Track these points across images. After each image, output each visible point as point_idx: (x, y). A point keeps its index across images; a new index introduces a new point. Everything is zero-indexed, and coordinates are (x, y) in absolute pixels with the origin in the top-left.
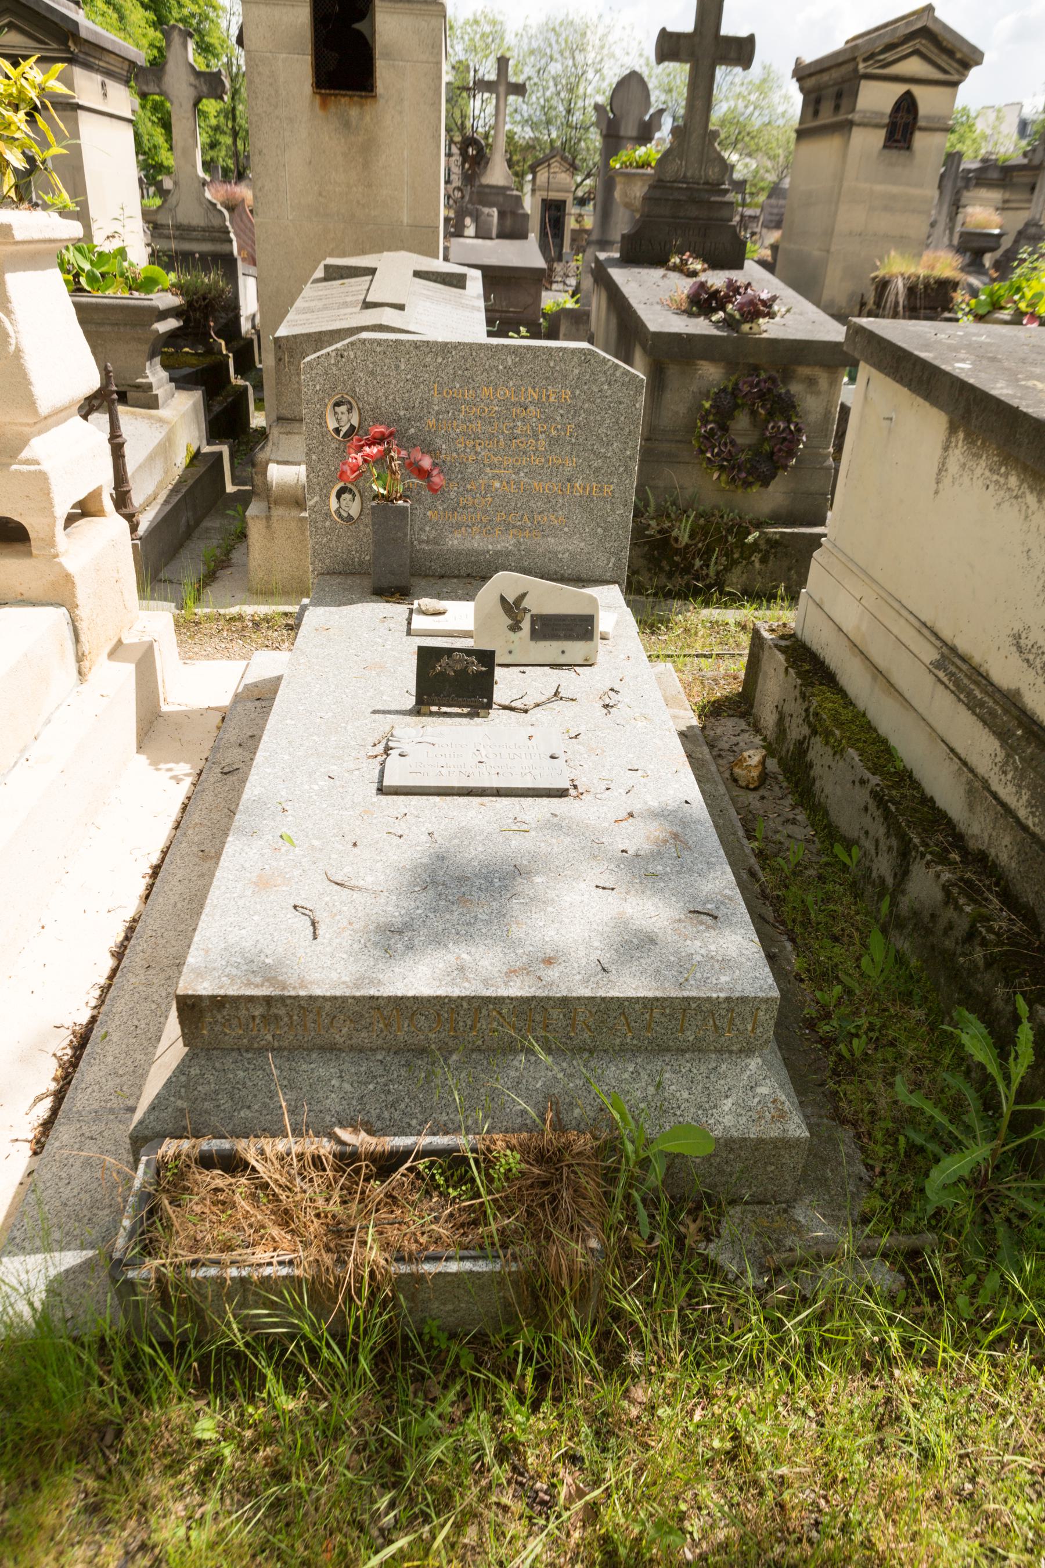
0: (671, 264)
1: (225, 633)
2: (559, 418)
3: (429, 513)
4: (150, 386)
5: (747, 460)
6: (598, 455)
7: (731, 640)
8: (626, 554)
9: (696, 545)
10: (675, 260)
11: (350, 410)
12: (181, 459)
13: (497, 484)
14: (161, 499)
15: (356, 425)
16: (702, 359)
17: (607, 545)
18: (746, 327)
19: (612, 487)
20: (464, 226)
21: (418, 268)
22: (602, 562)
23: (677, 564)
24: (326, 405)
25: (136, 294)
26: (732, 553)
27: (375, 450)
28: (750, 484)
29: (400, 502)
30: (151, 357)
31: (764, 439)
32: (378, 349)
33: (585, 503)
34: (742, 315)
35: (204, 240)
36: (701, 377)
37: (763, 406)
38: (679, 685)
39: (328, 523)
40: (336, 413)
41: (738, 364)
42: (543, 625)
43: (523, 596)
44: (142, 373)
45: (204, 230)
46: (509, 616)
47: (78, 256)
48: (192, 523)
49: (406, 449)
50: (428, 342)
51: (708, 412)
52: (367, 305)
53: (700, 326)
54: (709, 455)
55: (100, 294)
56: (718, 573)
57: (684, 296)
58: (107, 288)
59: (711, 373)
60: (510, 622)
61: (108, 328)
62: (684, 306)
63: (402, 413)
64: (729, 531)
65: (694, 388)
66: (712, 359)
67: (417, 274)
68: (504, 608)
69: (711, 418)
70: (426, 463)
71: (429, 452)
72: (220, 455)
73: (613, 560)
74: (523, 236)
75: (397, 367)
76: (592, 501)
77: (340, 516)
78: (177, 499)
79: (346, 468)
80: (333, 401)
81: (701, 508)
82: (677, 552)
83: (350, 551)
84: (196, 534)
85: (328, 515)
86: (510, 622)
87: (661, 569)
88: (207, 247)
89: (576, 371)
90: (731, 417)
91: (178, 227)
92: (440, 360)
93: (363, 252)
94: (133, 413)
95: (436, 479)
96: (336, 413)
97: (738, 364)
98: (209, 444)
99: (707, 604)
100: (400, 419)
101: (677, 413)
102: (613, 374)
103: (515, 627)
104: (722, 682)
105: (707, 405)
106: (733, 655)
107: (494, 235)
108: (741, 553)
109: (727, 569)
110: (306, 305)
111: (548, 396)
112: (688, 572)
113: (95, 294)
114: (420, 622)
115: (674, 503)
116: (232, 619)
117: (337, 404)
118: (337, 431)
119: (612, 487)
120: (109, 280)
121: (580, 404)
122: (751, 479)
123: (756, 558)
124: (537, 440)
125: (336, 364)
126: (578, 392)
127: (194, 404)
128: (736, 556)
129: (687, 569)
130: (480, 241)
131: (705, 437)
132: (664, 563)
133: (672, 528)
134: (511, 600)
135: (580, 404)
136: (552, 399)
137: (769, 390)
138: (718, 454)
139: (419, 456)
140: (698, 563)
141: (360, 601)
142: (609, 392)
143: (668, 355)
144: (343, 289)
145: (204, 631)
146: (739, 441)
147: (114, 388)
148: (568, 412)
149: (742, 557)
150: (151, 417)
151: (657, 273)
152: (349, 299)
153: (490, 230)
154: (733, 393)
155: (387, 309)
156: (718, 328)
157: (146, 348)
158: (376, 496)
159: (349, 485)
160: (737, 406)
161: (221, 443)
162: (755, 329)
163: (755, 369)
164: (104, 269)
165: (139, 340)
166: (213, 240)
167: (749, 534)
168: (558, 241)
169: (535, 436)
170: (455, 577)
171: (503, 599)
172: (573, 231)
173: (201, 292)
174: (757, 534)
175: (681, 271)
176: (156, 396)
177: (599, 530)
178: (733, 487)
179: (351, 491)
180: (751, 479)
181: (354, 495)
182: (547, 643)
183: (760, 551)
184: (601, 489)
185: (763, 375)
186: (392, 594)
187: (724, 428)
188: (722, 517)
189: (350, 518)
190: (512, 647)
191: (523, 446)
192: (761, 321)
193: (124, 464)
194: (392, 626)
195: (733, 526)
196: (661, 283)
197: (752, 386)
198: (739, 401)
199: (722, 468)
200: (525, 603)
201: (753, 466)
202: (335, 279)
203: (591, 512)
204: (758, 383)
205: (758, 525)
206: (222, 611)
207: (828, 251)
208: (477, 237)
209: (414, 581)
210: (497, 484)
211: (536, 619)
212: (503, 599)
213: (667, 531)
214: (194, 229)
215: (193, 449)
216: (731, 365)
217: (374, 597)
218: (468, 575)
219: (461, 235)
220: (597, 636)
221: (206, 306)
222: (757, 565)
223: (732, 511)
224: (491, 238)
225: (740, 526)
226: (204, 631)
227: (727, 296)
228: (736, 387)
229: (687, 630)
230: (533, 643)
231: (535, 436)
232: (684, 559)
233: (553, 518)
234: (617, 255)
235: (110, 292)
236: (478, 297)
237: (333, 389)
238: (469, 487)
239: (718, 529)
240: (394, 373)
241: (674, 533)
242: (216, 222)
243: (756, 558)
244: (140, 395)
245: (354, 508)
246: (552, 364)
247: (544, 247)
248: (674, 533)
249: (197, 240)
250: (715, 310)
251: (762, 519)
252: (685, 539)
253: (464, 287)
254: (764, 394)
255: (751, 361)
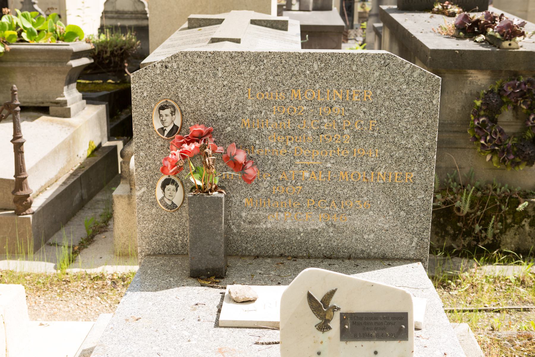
0: (435, 9)
1: (88, 290)
2: (362, 115)
3: (245, 201)
4: (65, 103)
5: (514, 145)
6: (399, 146)
7: (513, 294)
8: (428, 234)
9: (475, 213)
10: (438, 6)
11: (173, 113)
12: (83, 152)
13: (306, 174)
14: (60, 182)
15: (179, 125)
16: (475, 68)
17: (410, 227)
18: (506, 44)
19: (413, 175)
20: (292, 4)
21: (254, 18)
22: (405, 243)
23: (460, 229)
24: (152, 109)
25: (60, 42)
26: (506, 219)
27: (193, 146)
28: (518, 164)
29: (215, 194)
30: (69, 82)
31: (526, 128)
32: (198, 60)
33: (388, 189)
34: (502, 35)
35: (131, 19)
36: (471, 82)
37: (524, 103)
38: (479, 347)
39: (154, 211)
40: (161, 116)
41: (501, 71)
42: (353, 323)
43: (332, 293)
44: (61, 94)
45: (132, 13)
46: (318, 315)
47: (23, 19)
48: (85, 197)
49: (223, 145)
50: (242, 53)
51: (479, 109)
52: (214, 40)
53: (467, 45)
54: (483, 142)
55: (35, 43)
56: (494, 235)
57: (451, 26)
58: (40, 39)
59: (479, 79)
60: (318, 321)
61: (38, 65)
62: (453, 32)
63: (219, 114)
64: (503, 201)
65: (466, 91)
66: (480, 68)
67: (253, 22)
68: (312, 307)
69: (482, 113)
70: (241, 157)
71: (244, 147)
72: (115, 147)
73: (415, 240)
74: (329, 8)
75: (215, 75)
76: (395, 187)
77: (166, 206)
78: (73, 180)
79: (167, 163)
80: (158, 105)
81: (478, 184)
82: (459, 219)
83: (173, 235)
84: (88, 205)
85: (154, 203)
86: (318, 321)
87: (447, 233)
88: (133, 23)
89: (377, 74)
90: (499, 112)
91: (117, 12)
92: (253, 68)
93: (220, 13)
94: (51, 121)
95: (250, 171)
96: (161, 116)
97: (501, 71)
98: (109, 140)
99: (491, 261)
100: (218, 119)
101: (453, 110)
102: (411, 75)
103: (324, 327)
104: (518, 343)
105: (478, 103)
106: (518, 310)
107: (311, 7)
108: (514, 219)
109: (502, 232)
110: (171, 43)
111: (352, 96)
112: (469, 235)
113: (32, 43)
114: (231, 312)
115: (454, 180)
116: (97, 278)
117: (162, 108)
118: (162, 130)
119: (413, 175)
120: (41, 34)
121: (381, 102)
122: (518, 160)
123: (526, 223)
124: (343, 135)
125: (161, 74)
126: (379, 92)
127: (98, 114)
128: (509, 221)
129: (469, 232)
130: (302, 13)
131: (478, 128)
132: (449, 228)
133: (455, 200)
134: (319, 299)
135: (381, 102)
136: (355, 98)
137: (529, 90)
138: (489, 141)
139: (234, 151)
140: (478, 228)
141: (177, 284)
142: (408, 91)
143: (444, 64)
144: (200, 32)
145: (72, 289)
146: (506, 130)
147: (18, 103)
148: (371, 109)
149: (514, 221)
150: (64, 123)
151: (427, 16)
152: (201, 38)
153: (308, 6)
154: (499, 94)
155: (227, 42)
156: (483, 46)
157: (64, 77)
158: (193, 188)
159: (173, 177)
160: (502, 103)
161: (118, 139)
162: (514, 45)
163: (515, 75)
164: (40, 27)
165: (59, 72)
166: (137, 19)
167: (519, 203)
168: (351, 18)
169: (341, 131)
170: (269, 257)
171: (310, 297)
172: (360, 13)
173: (119, 45)
174: (526, 203)
175: (443, 14)
176: (69, 109)
177: (402, 213)
178: (503, 166)
179: (173, 182)
180: (518, 160)
181: (177, 186)
182: (358, 344)
183: (529, 217)
184: (403, 177)
185: (522, 80)
186: (208, 277)
187: (494, 121)
188: (495, 190)
189: (173, 206)
190: (320, 348)
191: (329, 140)
192: (518, 39)
193: (22, 158)
194: (202, 314)
195: (505, 197)
196: (430, 20)
197: (514, 87)
198: (505, 100)
199: (493, 152)
200: (334, 302)
201: (519, 149)
202: (195, 27)
203: (394, 197)
204: (520, 85)
205: (526, 196)
206: (89, 271)
207: (526, 11)
208: (300, 10)
209: (231, 261)
210: (306, 174)
211: (345, 318)
212: (310, 297)
213: (450, 203)
214: (126, 13)
215: (96, 144)
216: (495, 72)
217: (191, 280)
218: (281, 255)
219: (290, 10)
220: (411, 328)
221: (122, 54)
222: (527, 228)
223: (503, 185)
224: (309, 11)
225: (511, 197)
226: (72, 289)
227: (486, 23)
228: (501, 89)
229: (473, 286)
230: (343, 343)
231: (341, 131)
232: (466, 224)
233: (358, 203)
234: (396, 7)
235: (42, 42)
236: (296, 35)
237: (158, 95)
238: (281, 177)
239: (493, 200)
240: (212, 80)
241: (458, 204)
242: (139, 8)
243: (526, 223)
244: (59, 109)
245: (178, 197)
246: (354, 68)
247: (342, 15)
248: (458, 204)
249: (127, 19)
250: (478, 34)
251: (528, 191)
252: (466, 209)
253: (286, 30)
254: (525, 94)
255: (512, 69)
